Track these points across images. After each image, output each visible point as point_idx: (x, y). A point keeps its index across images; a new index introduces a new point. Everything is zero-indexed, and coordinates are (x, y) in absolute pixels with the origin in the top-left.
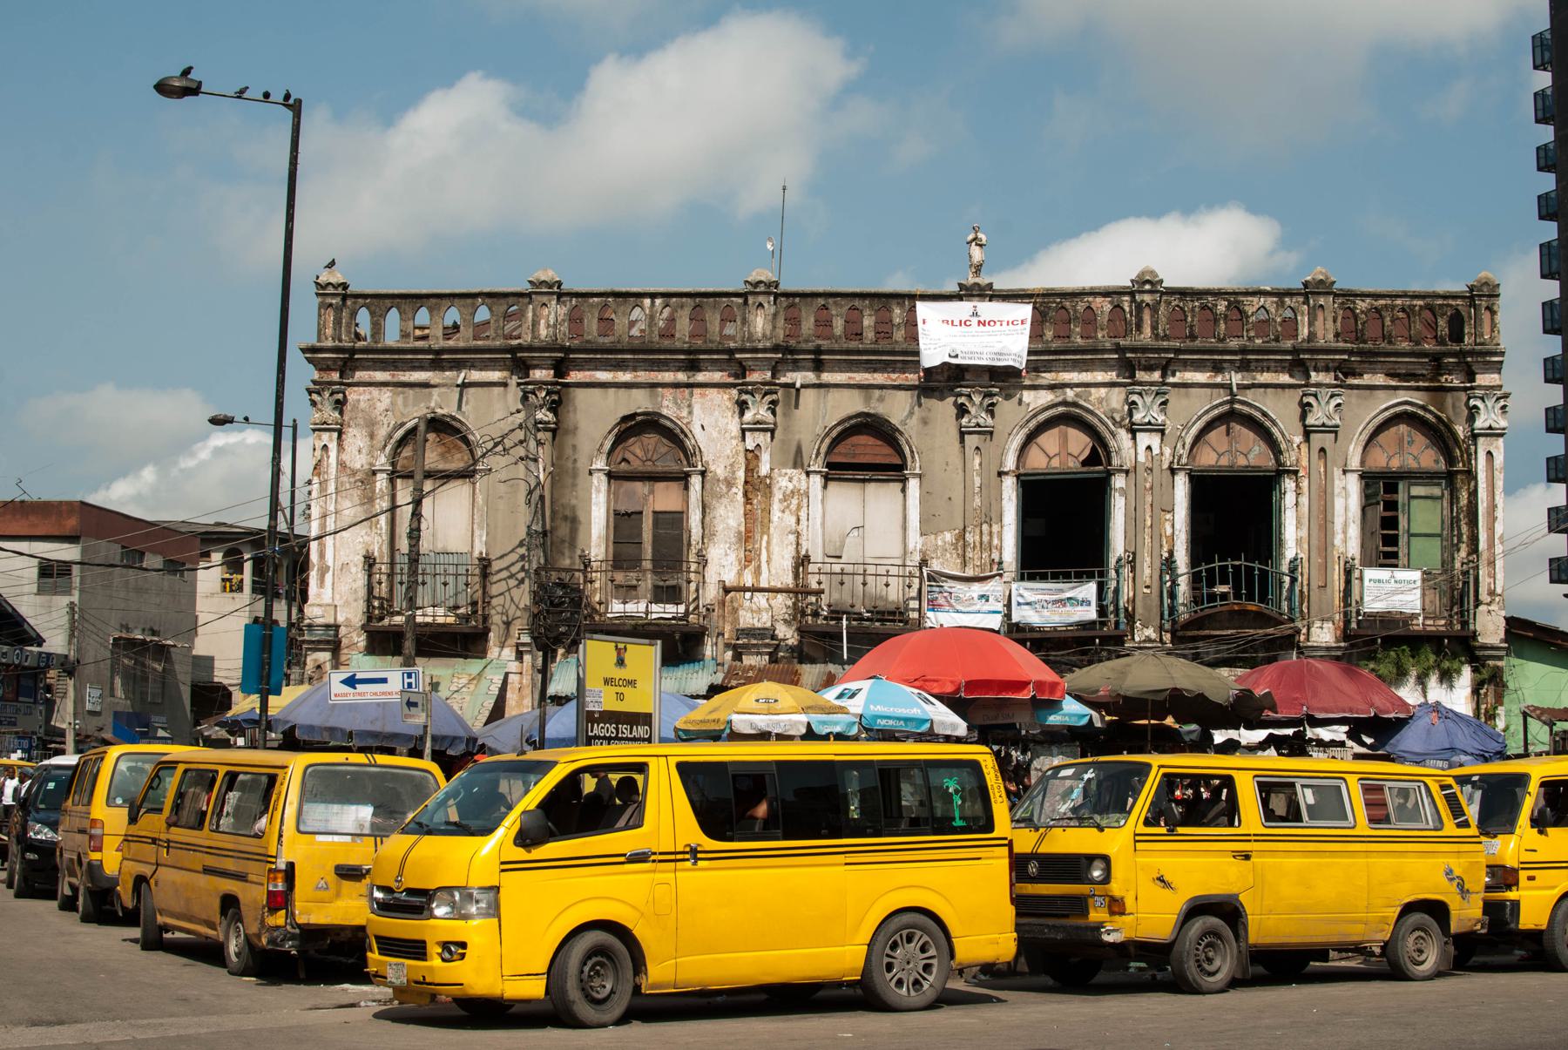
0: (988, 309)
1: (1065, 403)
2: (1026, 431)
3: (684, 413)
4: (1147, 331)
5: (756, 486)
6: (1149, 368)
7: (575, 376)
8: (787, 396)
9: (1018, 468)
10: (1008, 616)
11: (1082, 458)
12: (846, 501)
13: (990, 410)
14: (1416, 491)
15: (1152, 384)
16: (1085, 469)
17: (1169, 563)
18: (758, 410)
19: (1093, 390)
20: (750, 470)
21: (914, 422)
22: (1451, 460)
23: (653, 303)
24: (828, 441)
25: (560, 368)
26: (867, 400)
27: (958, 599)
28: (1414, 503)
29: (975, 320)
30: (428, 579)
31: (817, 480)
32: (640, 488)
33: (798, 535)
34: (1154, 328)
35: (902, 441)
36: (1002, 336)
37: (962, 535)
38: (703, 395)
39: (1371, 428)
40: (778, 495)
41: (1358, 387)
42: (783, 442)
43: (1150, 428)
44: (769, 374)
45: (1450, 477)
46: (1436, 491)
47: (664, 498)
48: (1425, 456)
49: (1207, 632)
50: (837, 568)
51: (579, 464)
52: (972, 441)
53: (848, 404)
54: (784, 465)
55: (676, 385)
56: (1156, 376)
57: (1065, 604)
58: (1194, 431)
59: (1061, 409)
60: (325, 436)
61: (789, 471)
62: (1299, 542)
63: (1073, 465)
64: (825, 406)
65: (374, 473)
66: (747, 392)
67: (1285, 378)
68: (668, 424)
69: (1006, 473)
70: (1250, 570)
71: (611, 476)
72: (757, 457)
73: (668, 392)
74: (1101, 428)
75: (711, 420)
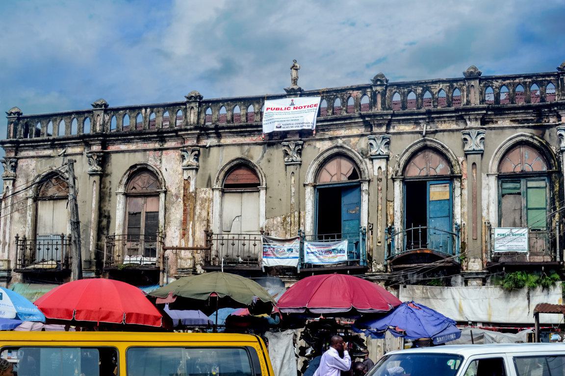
0: (299, 101)
1: (337, 147)
2: (317, 163)
3: (158, 163)
4: (379, 105)
5: (189, 198)
6: (380, 125)
7: (112, 148)
8: (204, 152)
9: (315, 181)
10: (302, 257)
11: (348, 175)
12: (232, 202)
13: (299, 152)
14: (530, 184)
15: (381, 133)
16: (351, 181)
17: (390, 231)
18: (190, 160)
19: (352, 139)
20: (186, 189)
21: (264, 161)
22: (549, 166)
23: (146, 111)
24: (223, 173)
25: (104, 145)
26: (145, 156)
27: (277, 251)
28: (530, 191)
29: (292, 107)
30: (41, 247)
31: (217, 194)
32: (140, 201)
33: (208, 221)
34: (383, 103)
35: (258, 172)
36: (302, 114)
37: (285, 219)
38: (167, 154)
39: (503, 151)
40: (199, 202)
41: (494, 128)
42: (202, 175)
43: (379, 157)
44: (195, 141)
45: (548, 175)
46: (543, 184)
47: (150, 205)
48: (537, 164)
49: (402, 266)
50: (230, 237)
51: (112, 191)
52: (291, 169)
53: (234, 153)
54: (202, 186)
55: (155, 150)
56: (384, 129)
58: (405, 157)
59: (336, 150)
60: (8, 182)
61: (205, 189)
62: (462, 215)
63: (344, 179)
64: (221, 155)
65: (27, 198)
66: (184, 151)
67: (454, 126)
68: (151, 169)
69: (307, 185)
70: (416, 231)
71: (127, 195)
72: (189, 183)
73: (151, 154)
74: (356, 159)
75: (171, 166)
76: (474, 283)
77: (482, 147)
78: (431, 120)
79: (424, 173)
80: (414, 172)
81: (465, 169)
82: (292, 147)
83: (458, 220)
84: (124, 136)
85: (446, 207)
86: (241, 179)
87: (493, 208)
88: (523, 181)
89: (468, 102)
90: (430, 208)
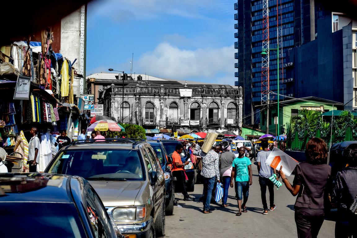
5: (162, 110)
10: (190, 124)
14: (233, 110)
22: (237, 107)
31: (168, 109)
33: (166, 115)
34: (205, 92)
46: (235, 110)
53: (172, 100)
57: (194, 123)
63: (196, 107)
75: (156, 102)
76: (223, 129)
77: (225, 103)
78: (215, 96)
79: (212, 107)
80: (211, 107)
81: (220, 107)
82: (186, 100)
83: (219, 117)
84: (145, 94)
85: (217, 114)
86: (174, 106)
87: (226, 115)
88: (231, 110)
89: (222, 94)
90: (214, 114)
